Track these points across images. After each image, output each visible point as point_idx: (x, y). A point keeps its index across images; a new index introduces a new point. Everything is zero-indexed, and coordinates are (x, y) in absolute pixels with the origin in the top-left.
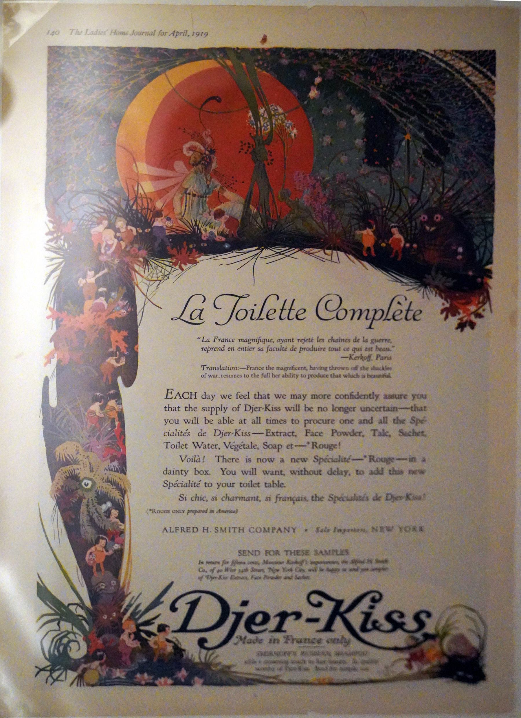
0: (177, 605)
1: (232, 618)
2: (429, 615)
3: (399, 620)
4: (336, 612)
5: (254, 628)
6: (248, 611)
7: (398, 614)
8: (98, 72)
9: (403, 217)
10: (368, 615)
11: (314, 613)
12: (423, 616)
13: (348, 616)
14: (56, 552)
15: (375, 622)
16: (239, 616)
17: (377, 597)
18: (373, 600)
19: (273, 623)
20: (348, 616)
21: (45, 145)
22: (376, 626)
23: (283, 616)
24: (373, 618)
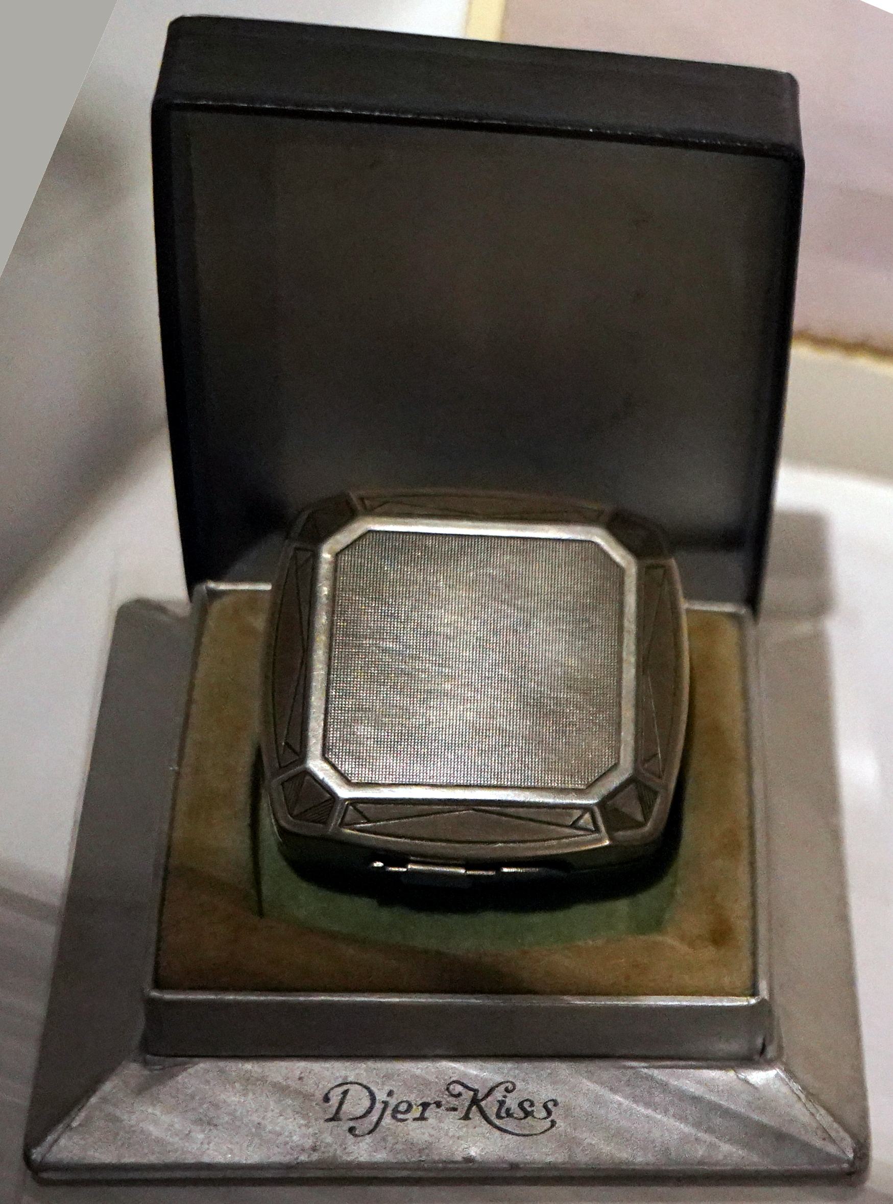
0: (330, 1095)
1: (379, 1106)
2: (556, 1103)
3: (529, 1109)
4: (475, 1101)
5: (400, 1116)
6: (393, 1102)
7: (552, 1103)
8: (725, 979)
9: (374, 642)
10: (502, 1103)
11: (454, 1102)
12: (550, 1105)
13: (483, 1103)
14: (395, 1054)
15: (508, 1110)
16: (386, 1104)
17: (510, 1086)
18: (507, 1090)
19: (416, 1112)
20: (483, 1103)
21: (500, 799)
22: (509, 1114)
23: (425, 1106)
24: (506, 1106)
